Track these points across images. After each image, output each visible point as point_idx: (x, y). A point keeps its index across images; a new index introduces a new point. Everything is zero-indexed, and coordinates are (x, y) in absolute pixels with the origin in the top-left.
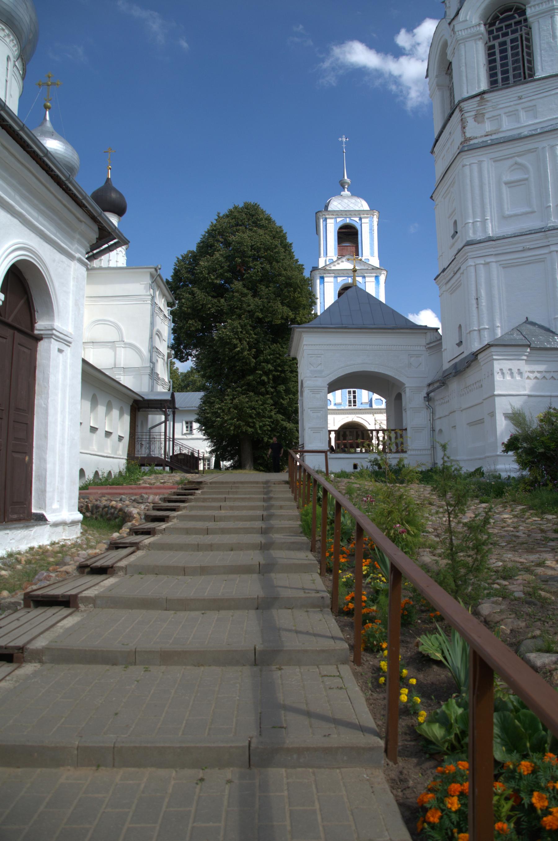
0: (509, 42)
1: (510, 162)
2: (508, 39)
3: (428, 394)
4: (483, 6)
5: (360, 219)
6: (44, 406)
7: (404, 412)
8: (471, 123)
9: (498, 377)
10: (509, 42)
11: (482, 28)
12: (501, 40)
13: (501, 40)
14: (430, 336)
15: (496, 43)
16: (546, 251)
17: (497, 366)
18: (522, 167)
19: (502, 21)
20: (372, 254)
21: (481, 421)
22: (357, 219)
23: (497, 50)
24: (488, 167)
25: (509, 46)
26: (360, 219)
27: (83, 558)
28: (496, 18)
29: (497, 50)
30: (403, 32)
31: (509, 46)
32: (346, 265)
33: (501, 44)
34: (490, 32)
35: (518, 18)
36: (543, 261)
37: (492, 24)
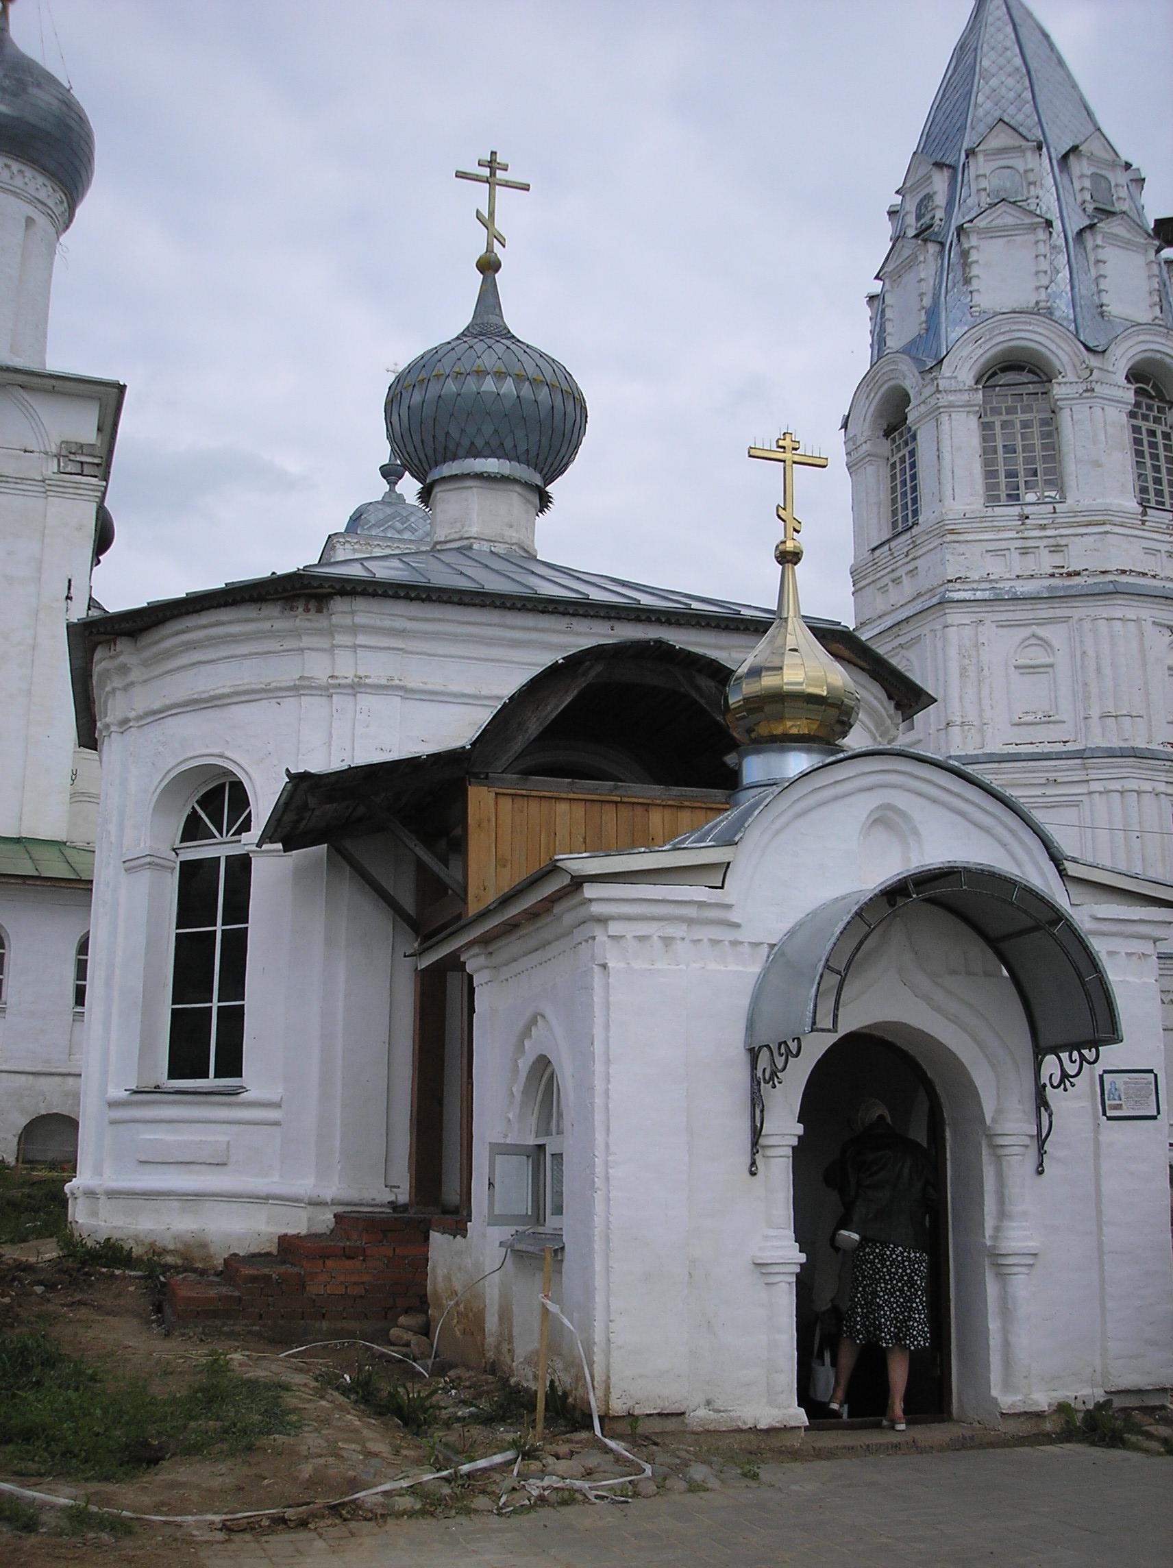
1: (1026, 632)
4: (982, 360)
16: (1082, 789)
18: (1044, 643)
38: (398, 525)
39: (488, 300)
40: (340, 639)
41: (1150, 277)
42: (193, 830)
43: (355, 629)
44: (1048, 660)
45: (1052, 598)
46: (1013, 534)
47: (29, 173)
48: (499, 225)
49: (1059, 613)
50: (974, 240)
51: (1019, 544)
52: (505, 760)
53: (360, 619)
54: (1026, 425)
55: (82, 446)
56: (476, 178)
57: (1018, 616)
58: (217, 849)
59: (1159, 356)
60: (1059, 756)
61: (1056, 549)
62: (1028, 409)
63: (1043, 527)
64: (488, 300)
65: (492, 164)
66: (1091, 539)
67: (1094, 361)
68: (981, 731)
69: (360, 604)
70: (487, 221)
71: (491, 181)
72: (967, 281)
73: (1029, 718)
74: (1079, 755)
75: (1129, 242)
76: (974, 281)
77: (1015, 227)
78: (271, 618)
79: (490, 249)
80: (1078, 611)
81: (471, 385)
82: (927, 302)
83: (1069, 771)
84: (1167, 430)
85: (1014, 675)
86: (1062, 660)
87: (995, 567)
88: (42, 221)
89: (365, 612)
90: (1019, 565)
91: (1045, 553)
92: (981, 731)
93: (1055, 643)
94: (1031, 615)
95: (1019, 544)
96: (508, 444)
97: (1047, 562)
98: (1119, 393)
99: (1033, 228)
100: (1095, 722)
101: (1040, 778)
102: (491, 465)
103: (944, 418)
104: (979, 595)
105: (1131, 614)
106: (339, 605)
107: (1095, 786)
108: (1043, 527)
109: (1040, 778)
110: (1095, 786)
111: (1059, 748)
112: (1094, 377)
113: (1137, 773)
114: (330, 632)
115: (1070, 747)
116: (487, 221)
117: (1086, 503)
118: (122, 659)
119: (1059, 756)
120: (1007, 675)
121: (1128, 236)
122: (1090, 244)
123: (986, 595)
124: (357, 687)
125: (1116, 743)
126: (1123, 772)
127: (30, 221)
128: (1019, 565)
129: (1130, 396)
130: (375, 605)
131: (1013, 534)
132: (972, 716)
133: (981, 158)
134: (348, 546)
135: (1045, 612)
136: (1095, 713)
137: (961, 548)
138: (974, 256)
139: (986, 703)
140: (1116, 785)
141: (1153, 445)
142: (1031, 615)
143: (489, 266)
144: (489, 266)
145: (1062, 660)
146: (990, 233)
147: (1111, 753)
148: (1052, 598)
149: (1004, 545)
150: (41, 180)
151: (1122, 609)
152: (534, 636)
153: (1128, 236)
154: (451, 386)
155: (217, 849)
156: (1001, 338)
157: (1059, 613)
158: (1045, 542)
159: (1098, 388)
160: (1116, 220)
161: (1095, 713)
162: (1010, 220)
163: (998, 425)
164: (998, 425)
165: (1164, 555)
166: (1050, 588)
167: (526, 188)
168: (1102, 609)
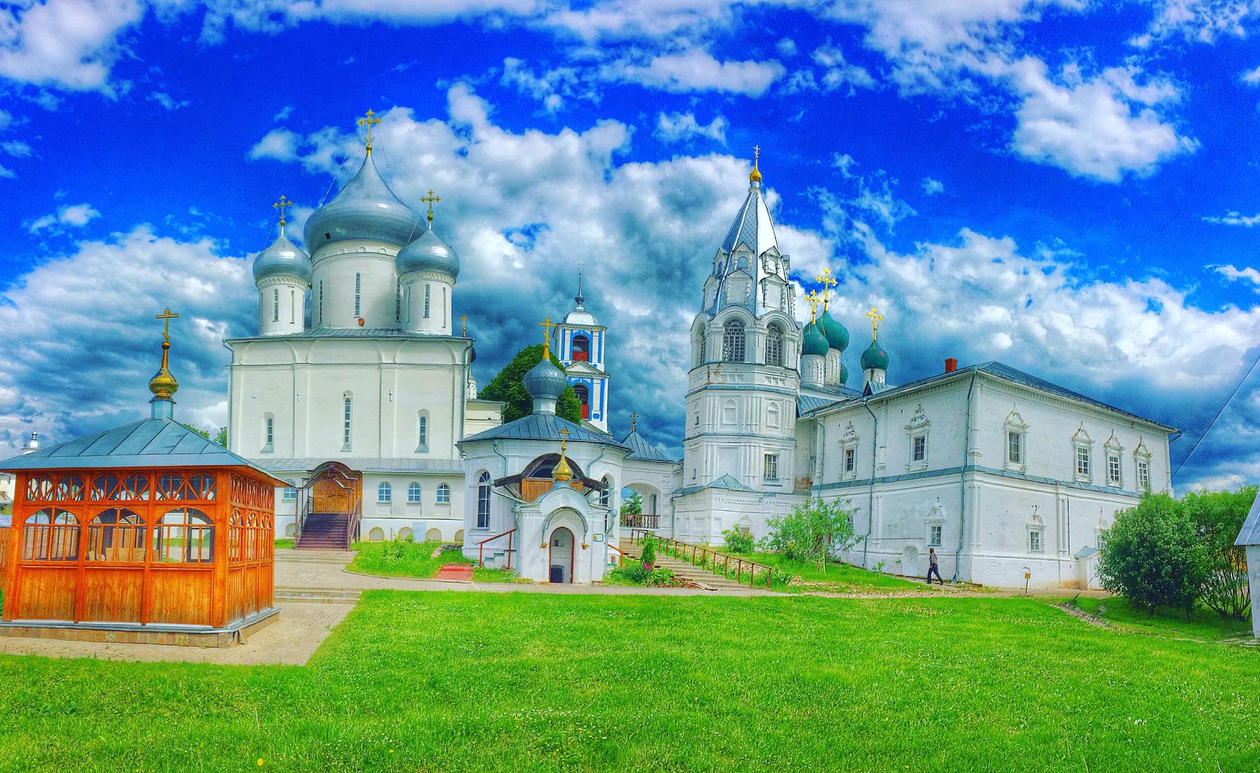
2: (735, 336)
5: (592, 332)
8: (712, 375)
15: (729, 336)
18: (733, 402)
19: (733, 326)
20: (599, 361)
22: (589, 333)
26: (592, 332)
34: (726, 330)
42: (481, 480)
58: (485, 484)
102: (552, 397)
129: (767, 332)
155: (485, 484)
167: (358, 275)
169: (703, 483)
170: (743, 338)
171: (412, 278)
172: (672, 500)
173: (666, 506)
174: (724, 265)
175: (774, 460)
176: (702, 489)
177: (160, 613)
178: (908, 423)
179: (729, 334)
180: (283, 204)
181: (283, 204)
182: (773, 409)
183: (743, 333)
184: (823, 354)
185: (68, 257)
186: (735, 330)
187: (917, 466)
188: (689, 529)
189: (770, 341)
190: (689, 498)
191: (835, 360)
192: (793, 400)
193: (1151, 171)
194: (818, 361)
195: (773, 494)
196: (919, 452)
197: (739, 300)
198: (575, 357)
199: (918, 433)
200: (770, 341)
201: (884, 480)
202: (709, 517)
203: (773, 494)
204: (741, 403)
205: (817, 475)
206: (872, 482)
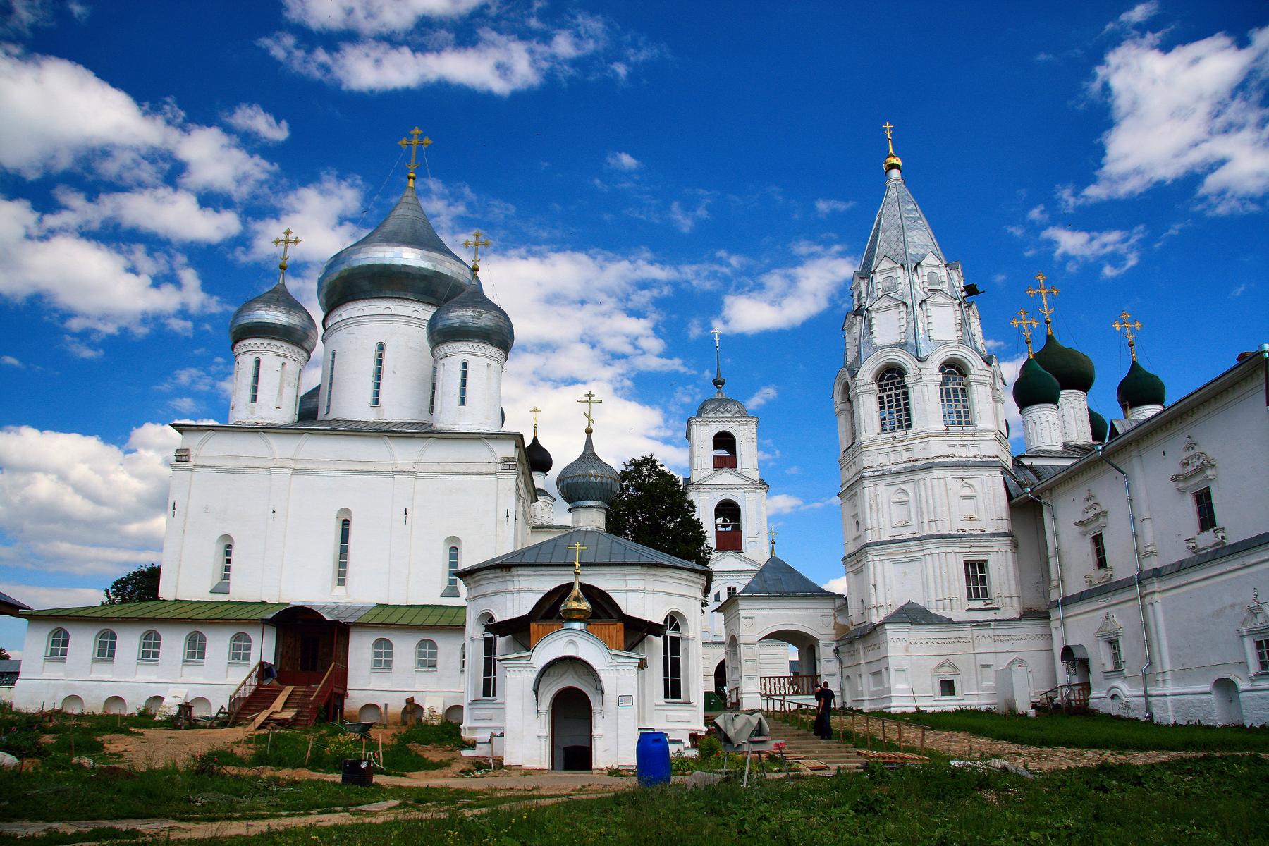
0: (893, 396)
1: (896, 487)
2: (893, 393)
3: (836, 648)
4: (875, 370)
6: (202, 800)
7: (817, 663)
9: (890, 644)
10: (893, 396)
11: (875, 386)
12: (888, 393)
13: (888, 393)
14: (838, 602)
15: (885, 394)
16: (921, 553)
17: (889, 636)
18: (905, 491)
21: (880, 672)
23: (885, 399)
24: (881, 489)
25: (893, 398)
27: (491, 449)
28: (883, 376)
29: (885, 399)
30: (796, 658)
31: (893, 398)
32: (726, 477)
33: (889, 396)
34: (880, 386)
35: (899, 379)
36: (920, 560)
37: (881, 380)
38: (722, 410)
39: (589, 443)
40: (515, 578)
41: (956, 317)
43: (518, 575)
44: (907, 499)
45: (907, 471)
46: (890, 446)
47: (486, 346)
48: (592, 417)
49: (910, 478)
50: (874, 314)
51: (892, 449)
52: (540, 617)
53: (519, 573)
54: (897, 395)
55: (508, 458)
56: (585, 401)
57: (894, 481)
59: (955, 356)
60: (911, 540)
61: (908, 450)
62: (897, 388)
63: (902, 441)
64: (589, 443)
65: (589, 395)
66: (922, 444)
67: (921, 365)
68: (879, 532)
69: (519, 569)
70: (588, 416)
71: (589, 401)
72: (871, 333)
73: (899, 525)
74: (919, 539)
75: (945, 303)
76: (874, 333)
77: (890, 307)
78: (498, 573)
79: (589, 424)
80: (917, 476)
81: (576, 480)
82: (857, 343)
83: (915, 546)
84: (963, 387)
85: (893, 506)
86: (912, 498)
87: (882, 460)
88: (494, 364)
89: (520, 571)
90: (893, 458)
91: (892, 454)
92: (879, 532)
93: (909, 491)
94: (898, 480)
95: (892, 449)
96: (589, 496)
97: (905, 456)
98: (934, 377)
99: (897, 306)
100: (926, 524)
101: (903, 550)
102: (590, 503)
103: (860, 397)
104: (876, 473)
105: (941, 475)
106: (514, 570)
107: (926, 552)
108: (902, 441)
109: (903, 550)
110: (926, 552)
111: (912, 536)
112: (922, 372)
113: (943, 545)
114: (513, 576)
115: (916, 536)
116: (588, 416)
117: (920, 429)
118: (469, 582)
119: (911, 540)
120: (890, 507)
121: (945, 300)
122: (924, 308)
123: (879, 473)
124: (519, 591)
125: (935, 532)
126: (938, 545)
127: (489, 365)
128: (893, 458)
129: (940, 377)
130: (523, 569)
131: (890, 446)
132: (875, 526)
133: (878, 274)
134: (697, 423)
135: (904, 478)
136: (926, 520)
137: (869, 453)
138: (874, 321)
139: (881, 519)
140: (935, 551)
141: (956, 396)
142: (898, 480)
143: (589, 431)
144: (589, 431)
145: (912, 498)
146: (880, 310)
147: (932, 537)
148: (907, 471)
149: (886, 450)
150: (491, 348)
151: (937, 473)
152: (567, 572)
153: (945, 300)
154: (570, 481)
156: (882, 360)
157: (910, 478)
158: (903, 447)
159: (923, 377)
160: (938, 294)
161: (926, 520)
162: (888, 304)
163: (885, 397)
164: (885, 397)
165: (959, 446)
166: (905, 468)
168: (927, 475)
169: (876, 620)
170: (906, 393)
171: (447, 351)
172: (837, 651)
173: (829, 661)
174: (864, 294)
175: (982, 571)
176: (875, 628)
177: (252, 826)
178: (1176, 469)
179: (884, 391)
180: (415, 141)
181: (415, 141)
182: (967, 492)
183: (904, 387)
184: (1053, 400)
185: (591, 16)
186: (893, 384)
187: (1207, 539)
188: (862, 692)
189: (947, 390)
190: (860, 646)
191: (1073, 403)
192: (998, 472)
193: (1218, 34)
194: (1042, 412)
195: (986, 624)
196: (1207, 519)
197: (894, 337)
198: (719, 463)
199: (1197, 483)
200: (947, 390)
201: (1157, 573)
202: (887, 669)
203: (986, 624)
204: (917, 489)
205: (1054, 583)
206: (1143, 579)
